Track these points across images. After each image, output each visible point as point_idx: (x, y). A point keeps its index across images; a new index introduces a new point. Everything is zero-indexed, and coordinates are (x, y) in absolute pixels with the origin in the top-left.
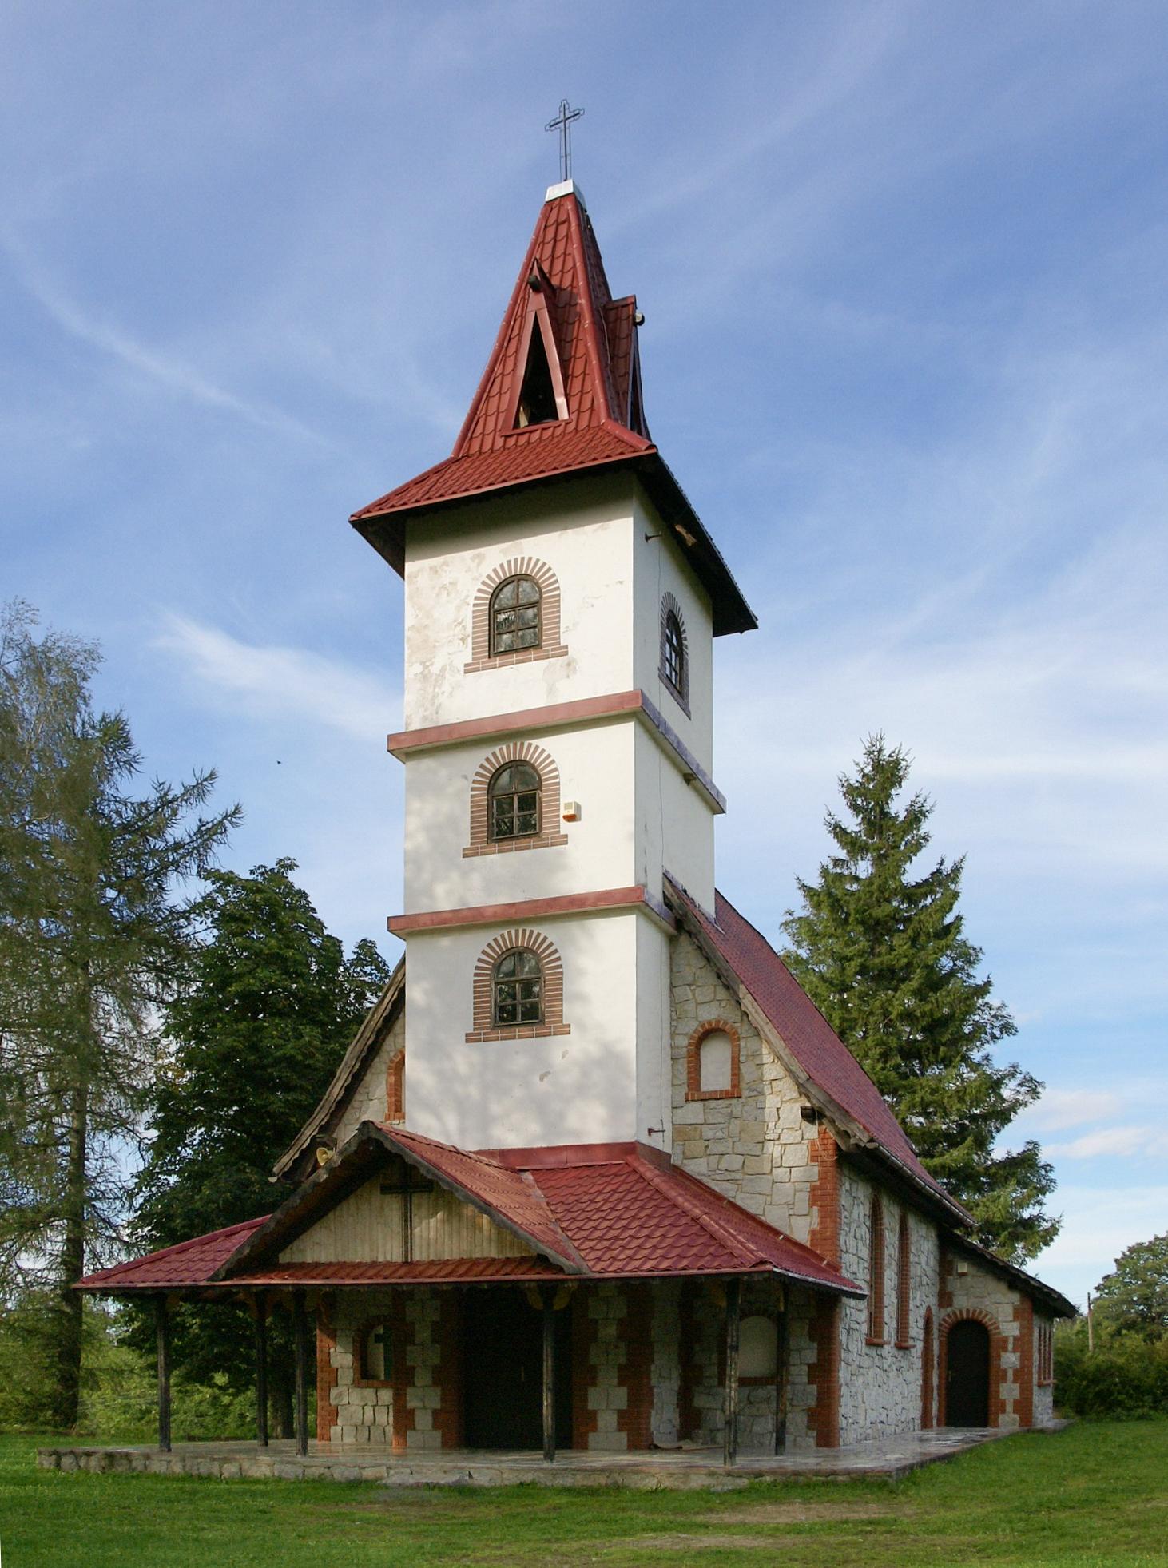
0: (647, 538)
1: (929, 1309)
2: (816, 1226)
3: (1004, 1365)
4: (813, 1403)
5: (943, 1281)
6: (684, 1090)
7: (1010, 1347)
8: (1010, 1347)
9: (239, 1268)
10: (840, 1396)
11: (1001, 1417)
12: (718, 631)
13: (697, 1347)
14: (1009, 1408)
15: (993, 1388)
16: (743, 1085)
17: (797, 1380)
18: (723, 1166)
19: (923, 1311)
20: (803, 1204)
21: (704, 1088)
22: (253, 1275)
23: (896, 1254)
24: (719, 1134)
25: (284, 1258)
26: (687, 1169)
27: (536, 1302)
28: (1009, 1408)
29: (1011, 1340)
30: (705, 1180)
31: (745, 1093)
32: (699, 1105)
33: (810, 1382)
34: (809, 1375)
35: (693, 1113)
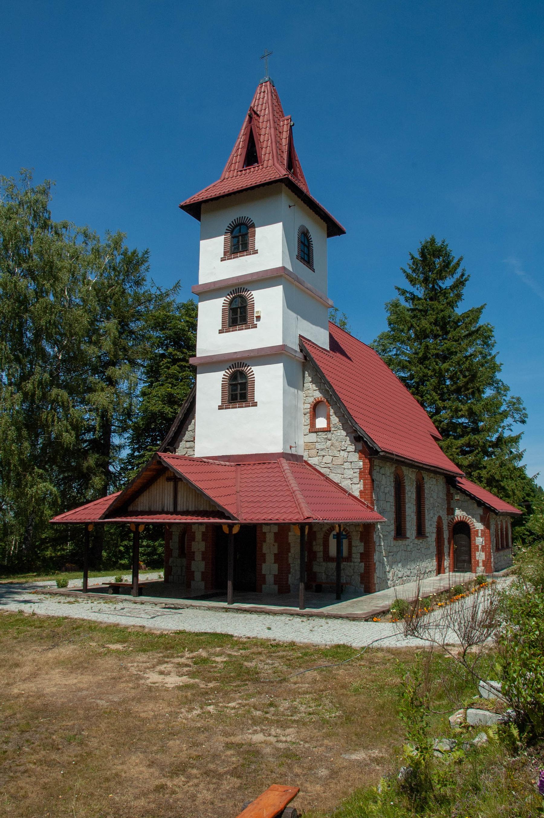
0: (290, 207)
1: (440, 518)
2: (362, 489)
3: (477, 544)
4: (362, 571)
5: (449, 503)
6: (308, 427)
7: (480, 535)
8: (480, 535)
9: (112, 512)
10: (375, 569)
11: (477, 568)
12: (329, 235)
13: (314, 543)
14: (481, 564)
15: (473, 554)
16: (331, 425)
17: (356, 560)
18: (324, 461)
19: (435, 519)
20: (356, 480)
21: (317, 427)
22: (120, 516)
23: (414, 496)
24: (323, 447)
25: (131, 508)
26: (309, 462)
27: (226, 529)
28: (481, 564)
29: (480, 531)
30: (317, 467)
31: (333, 429)
32: (314, 435)
33: (361, 562)
34: (361, 559)
35: (313, 437)
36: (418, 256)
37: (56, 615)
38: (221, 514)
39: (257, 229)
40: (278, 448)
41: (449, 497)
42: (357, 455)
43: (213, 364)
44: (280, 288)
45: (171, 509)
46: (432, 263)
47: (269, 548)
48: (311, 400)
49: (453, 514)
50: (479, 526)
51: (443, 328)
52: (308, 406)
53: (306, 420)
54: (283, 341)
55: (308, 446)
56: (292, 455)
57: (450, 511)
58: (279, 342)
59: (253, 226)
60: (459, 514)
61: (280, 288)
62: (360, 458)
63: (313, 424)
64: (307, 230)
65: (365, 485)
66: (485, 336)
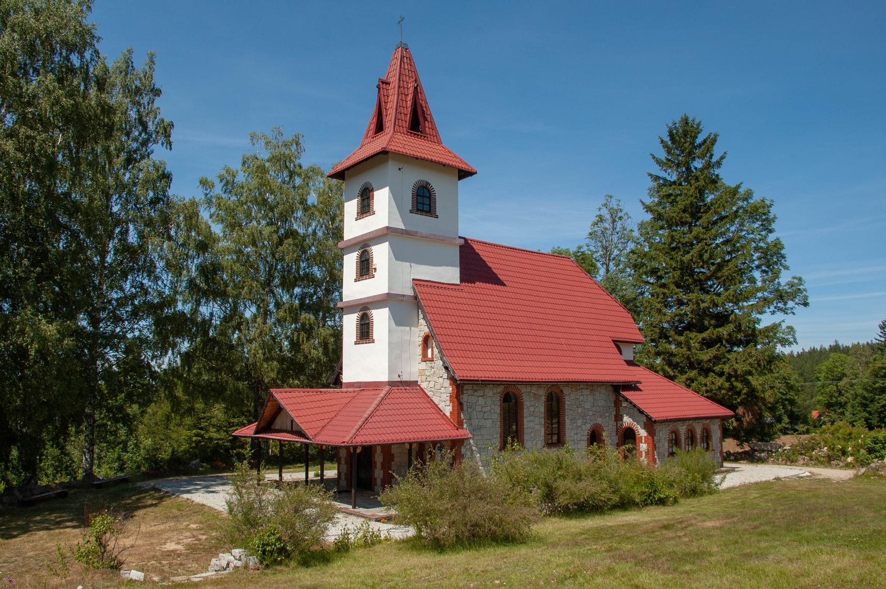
5: (618, 410)
20: (448, 403)
36: (667, 139)
37: (753, 481)
38: (301, 434)
39: (376, 193)
40: (385, 378)
41: (617, 404)
42: (448, 382)
43: (352, 307)
44: (386, 244)
45: (289, 428)
46: (686, 144)
47: (379, 458)
48: (422, 334)
49: (622, 420)
50: (642, 433)
51: (693, 215)
52: (421, 339)
53: (419, 351)
54: (389, 288)
55: (422, 372)
56: (401, 382)
57: (618, 418)
58: (385, 290)
59: (372, 190)
60: (627, 420)
61: (386, 244)
62: (451, 384)
63: (424, 354)
64: (428, 183)
65: (453, 407)
66: (761, 214)
